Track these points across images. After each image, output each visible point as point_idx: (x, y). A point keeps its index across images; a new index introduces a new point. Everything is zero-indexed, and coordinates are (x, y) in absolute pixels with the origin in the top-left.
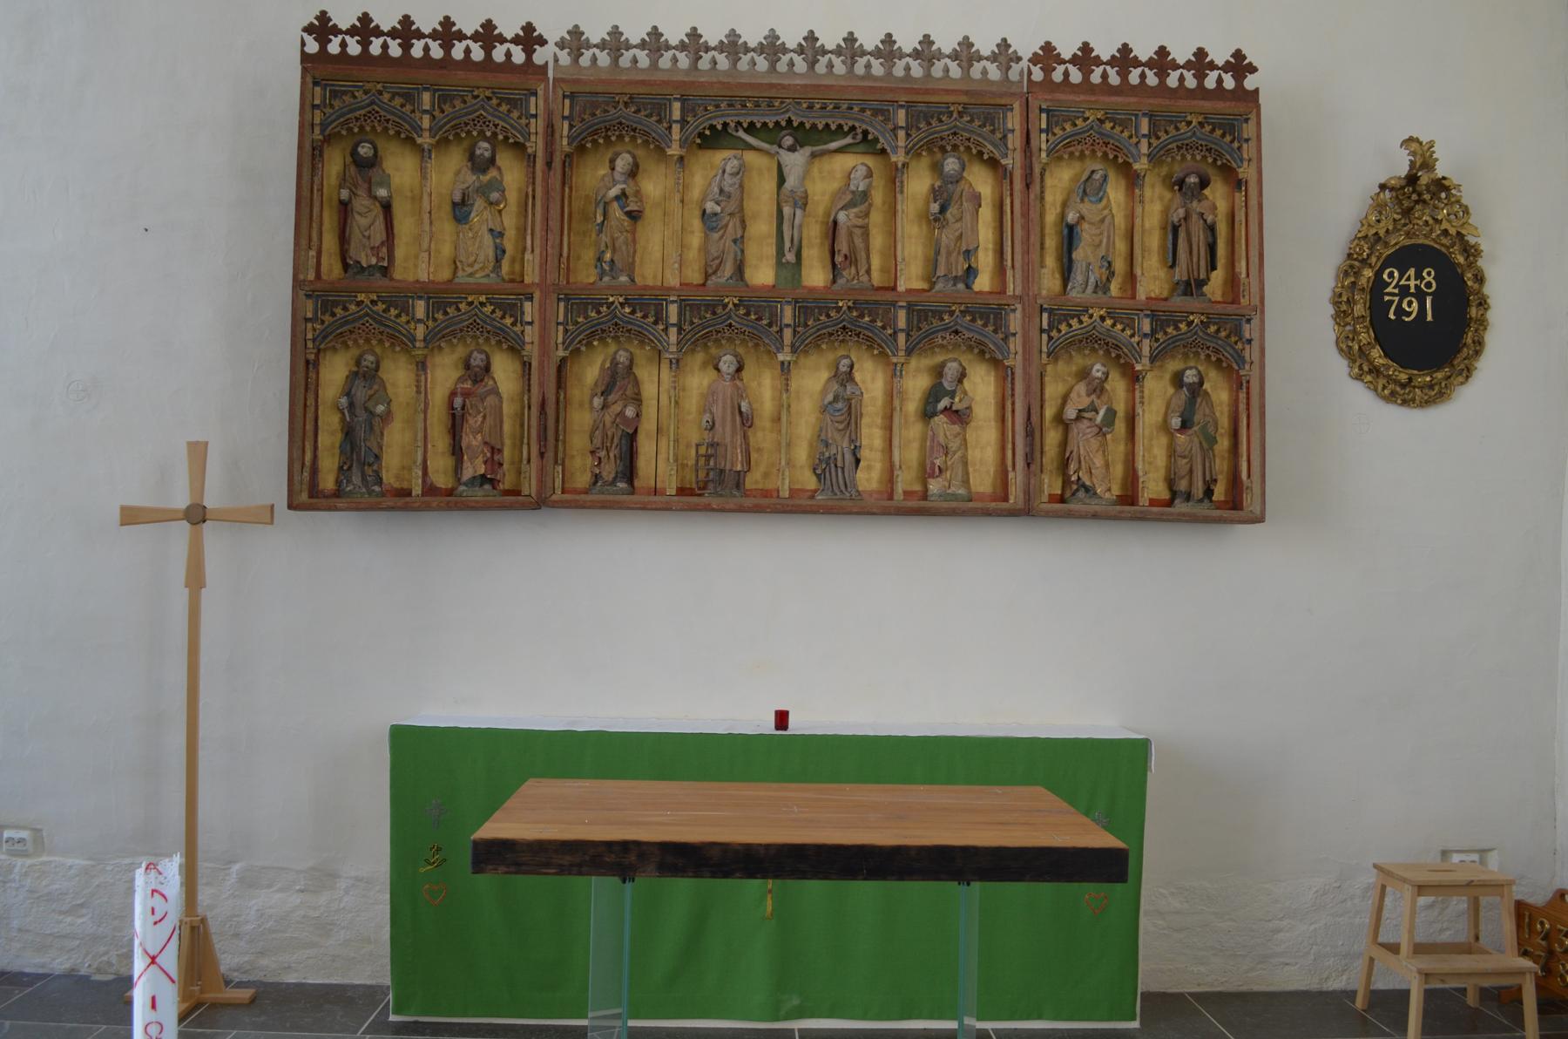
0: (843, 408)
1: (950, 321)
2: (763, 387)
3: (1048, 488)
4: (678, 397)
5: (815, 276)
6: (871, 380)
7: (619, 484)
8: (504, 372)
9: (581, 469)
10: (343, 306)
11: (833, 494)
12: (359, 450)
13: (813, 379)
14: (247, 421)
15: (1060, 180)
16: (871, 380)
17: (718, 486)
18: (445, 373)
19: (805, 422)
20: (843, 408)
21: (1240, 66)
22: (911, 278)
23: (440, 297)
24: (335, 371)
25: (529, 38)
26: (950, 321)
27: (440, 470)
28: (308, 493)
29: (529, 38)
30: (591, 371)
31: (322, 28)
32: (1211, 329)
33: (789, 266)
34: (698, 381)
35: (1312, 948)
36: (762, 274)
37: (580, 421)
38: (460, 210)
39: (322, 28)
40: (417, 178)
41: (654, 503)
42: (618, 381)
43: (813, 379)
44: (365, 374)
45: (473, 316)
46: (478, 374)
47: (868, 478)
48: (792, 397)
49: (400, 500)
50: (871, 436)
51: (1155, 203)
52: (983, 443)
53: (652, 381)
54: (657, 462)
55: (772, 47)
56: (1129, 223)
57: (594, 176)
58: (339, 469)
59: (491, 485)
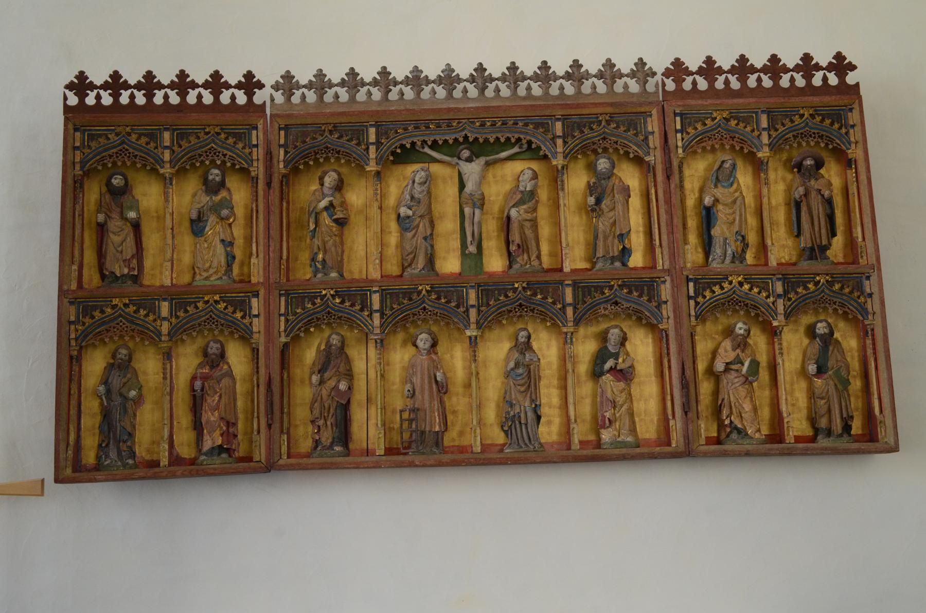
0: (524, 373)
1: (610, 294)
4: (384, 371)
5: (495, 263)
6: (546, 347)
7: (336, 448)
8: (237, 359)
10: (101, 309)
11: (519, 447)
13: (497, 350)
15: (696, 171)
16: (546, 347)
17: (421, 445)
18: (187, 361)
19: (493, 386)
20: (524, 373)
21: (841, 65)
22: (575, 259)
23: (181, 298)
24: (95, 364)
26: (610, 294)
28: (72, 467)
30: (309, 354)
31: (81, 85)
34: (400, 356)
36: (450, 264)
38: (197, 226)
39: (81, 85)
42: (334, 361)
43: (497, 350)
44: (121, 366)
45: (210, 312)
46: (215, 360)
47: (549, 432)
49: (150, 470)
50: (549, 395)
51: (779, 185)
52: (646, 396)
53: (363, 359)
54: (367, 427)
56: (759, 200)
57: (309, 191)
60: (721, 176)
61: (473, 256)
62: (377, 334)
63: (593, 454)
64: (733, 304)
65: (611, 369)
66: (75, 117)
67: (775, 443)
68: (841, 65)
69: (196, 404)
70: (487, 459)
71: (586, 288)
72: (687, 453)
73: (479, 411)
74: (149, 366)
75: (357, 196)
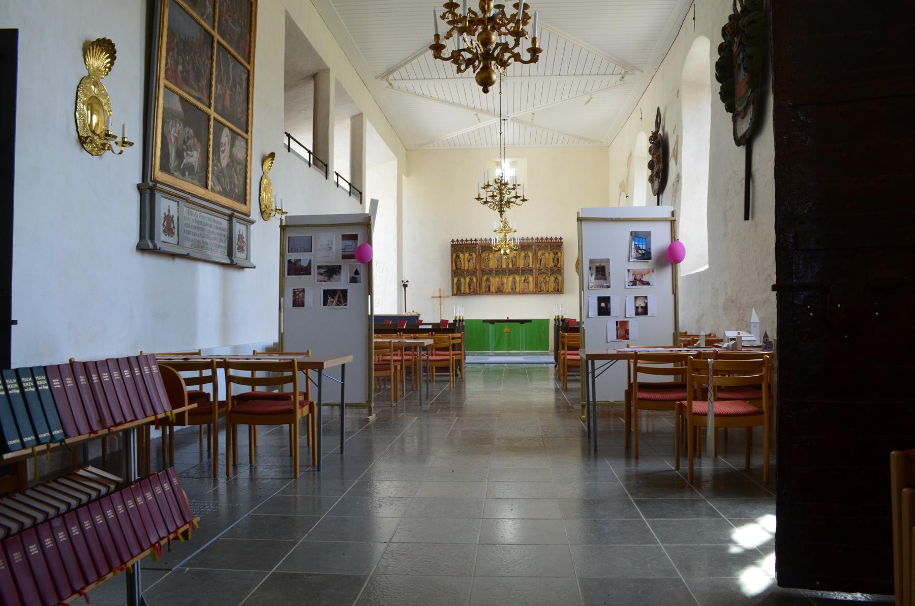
0: (514, 282)
1: (526, 271)
2: (505, 280)
3: (539, 290)
4: (495, 281)
5: (510, 266)
6: (518, 278)
7: (488, 292)
8: (474, 279)
9: (483, 290)
10: (457, 272)
11: (513, 292)
12: (459, 288)
13: (511, 279)
14: (447, 288)
15: (540, 253)
16: (518, 278)
17: (500, 292)
18: (468, 279)
19: (510, 283)
20: (514, 282)
21: (561, 239)
22: (522, 266)
23: (468, 271)
24: (455, 280)
25: (476, 240)
26: (526, 271)
27: (467, 291)
28: (453, 295)
29: (476, 240)
30: (485, 278)
31: (453, 241)
32: (557, 270)
33: (507, 266)
34: (497, 279)
35: (756, 598)
36: (504, 266)
37: (483, 285)
38: (469, 261)
39: (453, 241)
40: (465, 256)
41: (492, 294)
42: (488, 280)
43: (511, 279)
44: (459, 280)
45: (471, 273)
46: (471, 280)
47: (517, 290)
48: (508, 281)
49: (464, 294)
50: (517, 285)
51: (552, 255)
52: (531, 285)
53: (492, 279)
54: (493, 289)
55: (528, 239)
56: (548, 257)
57: (484, 255)
58: (458, 291)
59: (475, 291)
60: (543, 254)
61: (507, 266)
62: (188, 240)
63: (523, 293)
64: (543, 273)
65: (104, 428)
66: (452, 245)
67: (548, 292)
68: (561, 239)
69: (469, 286)
70: (509, 293)
71: (523, 271)
72: (536, 293)
73: (508, 287)
74: (462, 280)
75: (491, 256)
